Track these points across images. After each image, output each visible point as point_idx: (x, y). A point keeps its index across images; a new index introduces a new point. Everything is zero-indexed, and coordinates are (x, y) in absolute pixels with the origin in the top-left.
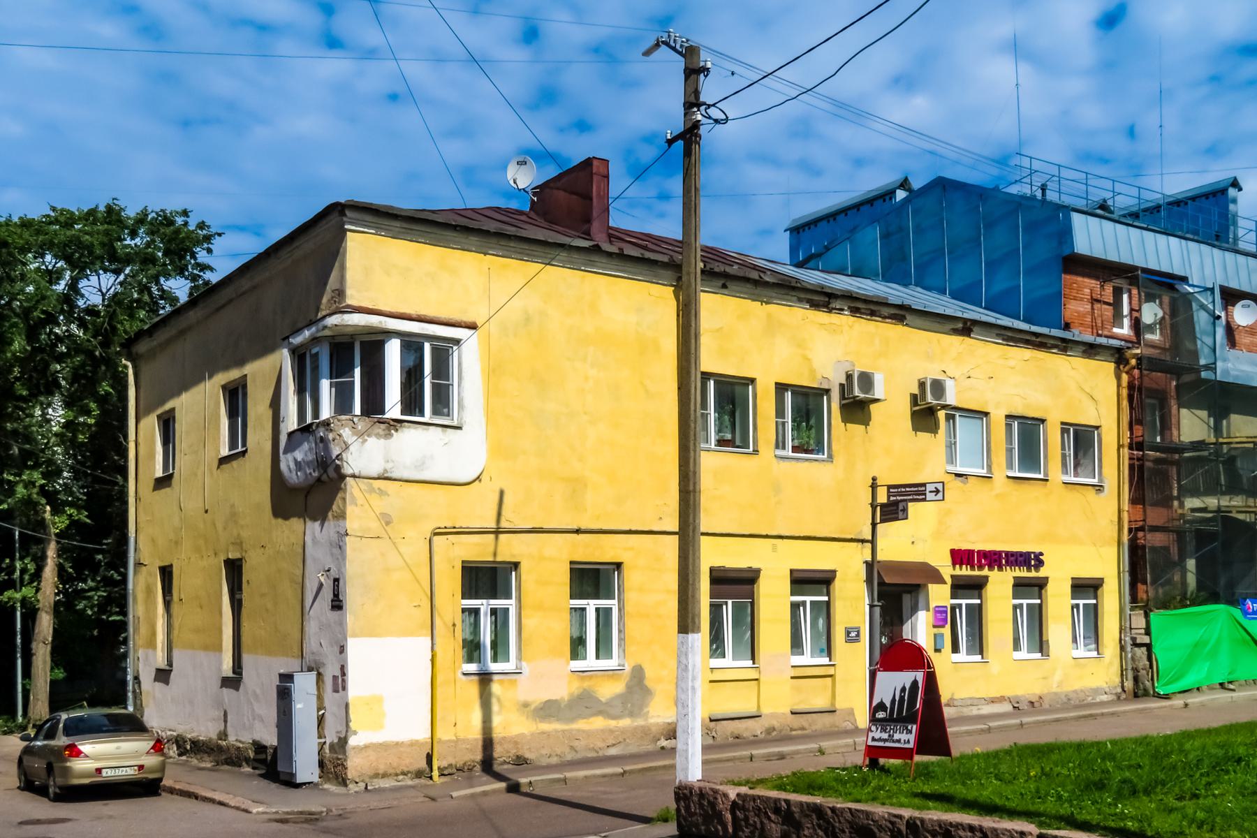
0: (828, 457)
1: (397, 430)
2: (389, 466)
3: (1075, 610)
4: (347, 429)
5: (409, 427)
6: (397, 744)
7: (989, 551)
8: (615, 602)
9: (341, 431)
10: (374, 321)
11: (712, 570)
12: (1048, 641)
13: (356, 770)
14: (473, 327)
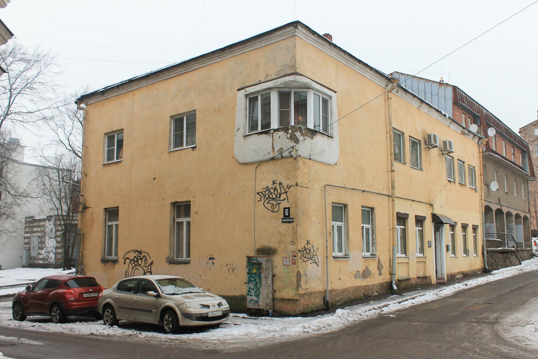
1: (315, 136)
2: (312, 152)
4: (298, 132)
9: (295, 133)
10: (308, 81)
14: (335, 92)
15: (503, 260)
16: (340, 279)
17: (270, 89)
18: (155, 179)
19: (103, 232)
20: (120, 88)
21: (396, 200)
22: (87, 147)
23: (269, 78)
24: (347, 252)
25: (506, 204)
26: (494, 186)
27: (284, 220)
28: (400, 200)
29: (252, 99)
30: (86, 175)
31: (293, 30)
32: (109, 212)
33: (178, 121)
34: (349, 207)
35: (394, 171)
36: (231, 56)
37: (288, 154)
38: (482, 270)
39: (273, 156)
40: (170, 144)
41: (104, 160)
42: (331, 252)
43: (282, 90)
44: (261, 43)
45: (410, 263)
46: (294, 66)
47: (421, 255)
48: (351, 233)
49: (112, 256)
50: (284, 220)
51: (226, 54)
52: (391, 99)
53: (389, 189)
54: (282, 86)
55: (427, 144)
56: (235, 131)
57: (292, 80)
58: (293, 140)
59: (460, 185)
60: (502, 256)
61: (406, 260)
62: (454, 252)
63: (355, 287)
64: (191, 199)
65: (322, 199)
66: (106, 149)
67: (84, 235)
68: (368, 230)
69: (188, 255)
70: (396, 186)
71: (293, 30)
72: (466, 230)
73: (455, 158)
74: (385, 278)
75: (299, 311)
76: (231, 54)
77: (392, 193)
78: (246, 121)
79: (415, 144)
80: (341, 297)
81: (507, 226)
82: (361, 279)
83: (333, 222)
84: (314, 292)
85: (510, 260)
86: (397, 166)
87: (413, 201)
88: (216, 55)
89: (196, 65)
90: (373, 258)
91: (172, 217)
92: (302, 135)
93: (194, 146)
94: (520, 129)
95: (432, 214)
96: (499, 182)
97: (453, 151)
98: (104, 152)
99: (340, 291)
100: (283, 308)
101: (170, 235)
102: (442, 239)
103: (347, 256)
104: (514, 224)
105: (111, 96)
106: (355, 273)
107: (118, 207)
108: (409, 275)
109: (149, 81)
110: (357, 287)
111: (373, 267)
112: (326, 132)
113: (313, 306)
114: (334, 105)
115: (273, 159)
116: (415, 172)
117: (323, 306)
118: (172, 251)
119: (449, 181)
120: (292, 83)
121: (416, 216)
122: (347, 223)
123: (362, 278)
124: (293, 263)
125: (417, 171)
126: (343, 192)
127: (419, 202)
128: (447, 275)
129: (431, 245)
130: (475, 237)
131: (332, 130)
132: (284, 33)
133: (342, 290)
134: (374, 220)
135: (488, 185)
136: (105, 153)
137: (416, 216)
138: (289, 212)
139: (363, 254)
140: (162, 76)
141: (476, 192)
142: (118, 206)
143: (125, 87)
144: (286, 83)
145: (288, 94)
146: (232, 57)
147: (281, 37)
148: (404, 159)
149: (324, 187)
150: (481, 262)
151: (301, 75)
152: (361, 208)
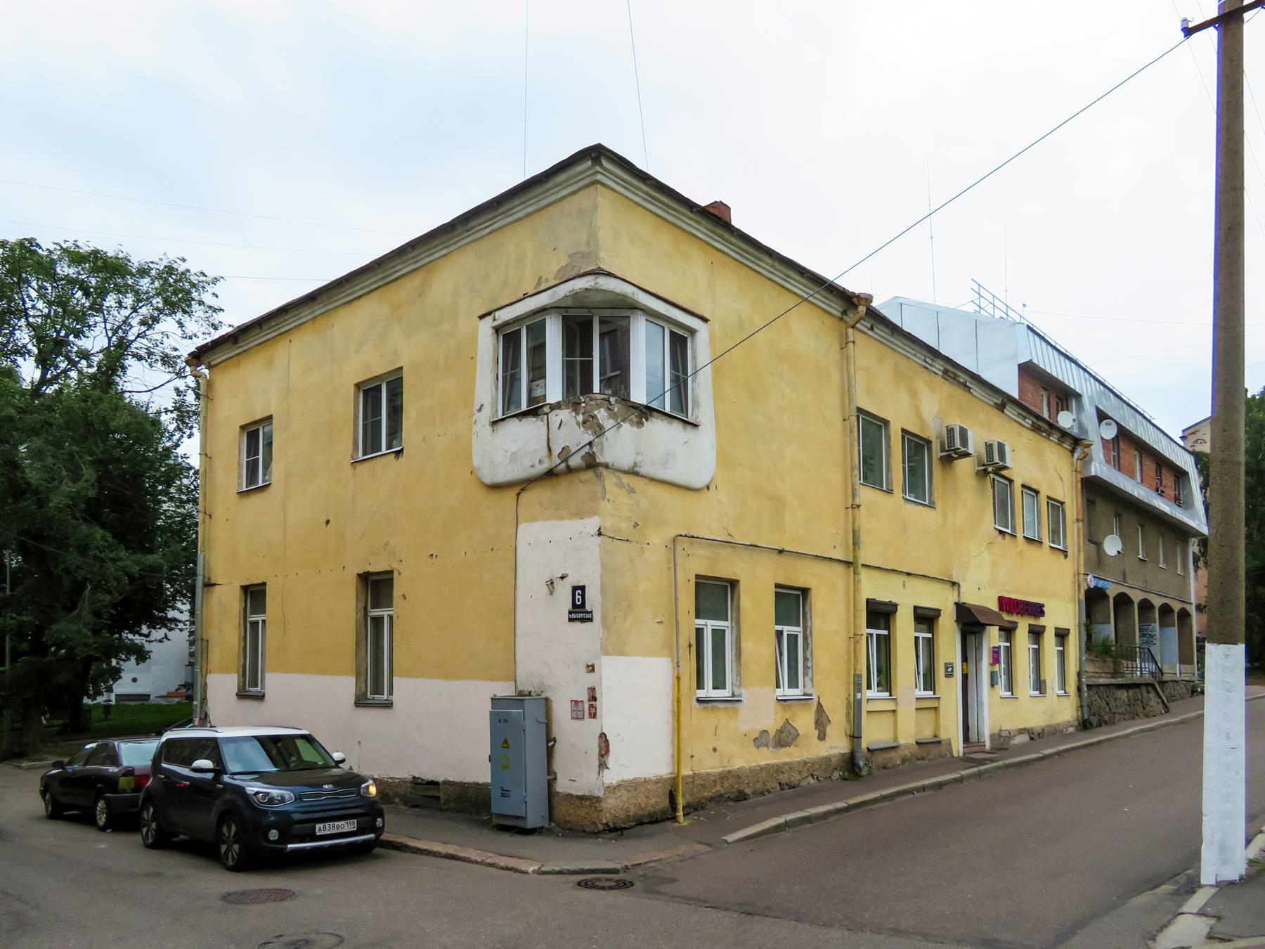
0: (929, 503)
1: (647, 420)
2: (639, 459)
3: (869, 638)
4: (602, 410)
5: (657, 418)
6: (645, 781)
7: (1014, 600)
8: (800, 629)
9: (596, 412)
10: (628, 290)
11: (868, 601)
12: (1045, 681)
13: (610, 814)
14: (705, 320)
15: (1128, 703)
16: (715, 750)
17: (543, 310)
18: (328, 522)
19: (239, 638)
20: (264, 328)
21: (864, 573)
22: (210, 458)
23: (543, 286)
24: (736, 689)
25: (1140, 584)
26: (1112, 546)
27: (573, 616)
28: (876, 574)
29: (508, 336)
30: (210, 516)
31: (590, 168)
32: (252, 592)
33: (369, 392)
34: (743, 587)
35: (859, 506)
36: (468, 240)
37: (581, 460)
38: (1077, 724)
39: (550, 467)
40: (356, 446)
41: (240, 484)
42: (692, 690)
43: (571, 313)
44: (526, 204)
45: (900, 711)
46: (590, 255)
47: (930, 694)
48: (746, 646)
49: (257, 687)
50: (573, 616)
51: (458, 236)
52: (854, 342)
53: (847, 547)
54: (569, 303)
55: (947, 448)
56: (475, 411)
57: (587, 286)
58: (590, 428)
59: (1028, 542)
60: (1126, 694)
61: (890, 706)
62: (1010, 686)
63: (755, 766)
64: (395, 566)
65: (669, 568)
66: (245, 460)
67: (208, 641)
68: (793, 639)
69: (391, 693)
70: (864, 537)
71: (590, 168)
72: (1040, 639)
73: (1015, 482)
74: (836, 745)
75: (602, 824)
76: (468, 236)
77: (854, 556)
78: (497, 389)
79: (916, 445)
80: (717, 791)
81: (1140, 630)
82: (771, 748)
83: (700, 622)
84: (619, 786)
85: (1142, 702)
86: (867, 495)
87: (909, 574)
88: (438, 242)
89: (400, 266)
90: (803, 702)
91: (362, 605)
92: (612, 415)
93: (399, 448)
94: (1184, 431)
95: (956, 604)
96: (1122, 537)
97: (1007, 465)
98: (240, 465)
99: (715, 776)
100: (571, 815)
101: (357, 644)
102: (981, 659)
103: (738, 696)
104: (1157, 625)
105: (251, 345)
106: (757, 735)
107: (264, 584)
108: (896, 738)
109: (317, 308)
110: (759, 766)
111: (804, 721)
112: (681, 414)
113: (641, 813)
114: (701, 350)
115: (550, 474)
116: (917, 512)
117: (670, 812)
118: (363, 679)
119: (1001, 532)
120: (589, 294)
121: (916, 608)
122: (737, 622)
123: (775, 747)
124: (590, 714)
125: (920, 508)
126: (725, 552)
127: (924, 576)
128: (992, 737)
129: (952, 671)
130: (1062, 655)
131: (695, 408)
132: (573, 177)
133: (720, 774)
134: (808, 616)
135: (1098, 545)
136: (242, 467)
137: (916, 608)
138: (583, 596)
139: (779, 692)
140: (340, 296)
141: (1066, 556)
142: (265, 581)
143: (273, 324)
144: (575, 295)
145: (586, 326)
146: (470, 242)
147: (566, 187)
148: (890, 481)
149: (674, 541)
150: (1074, 706)
151: (610, 275)
152: (773, 590)
